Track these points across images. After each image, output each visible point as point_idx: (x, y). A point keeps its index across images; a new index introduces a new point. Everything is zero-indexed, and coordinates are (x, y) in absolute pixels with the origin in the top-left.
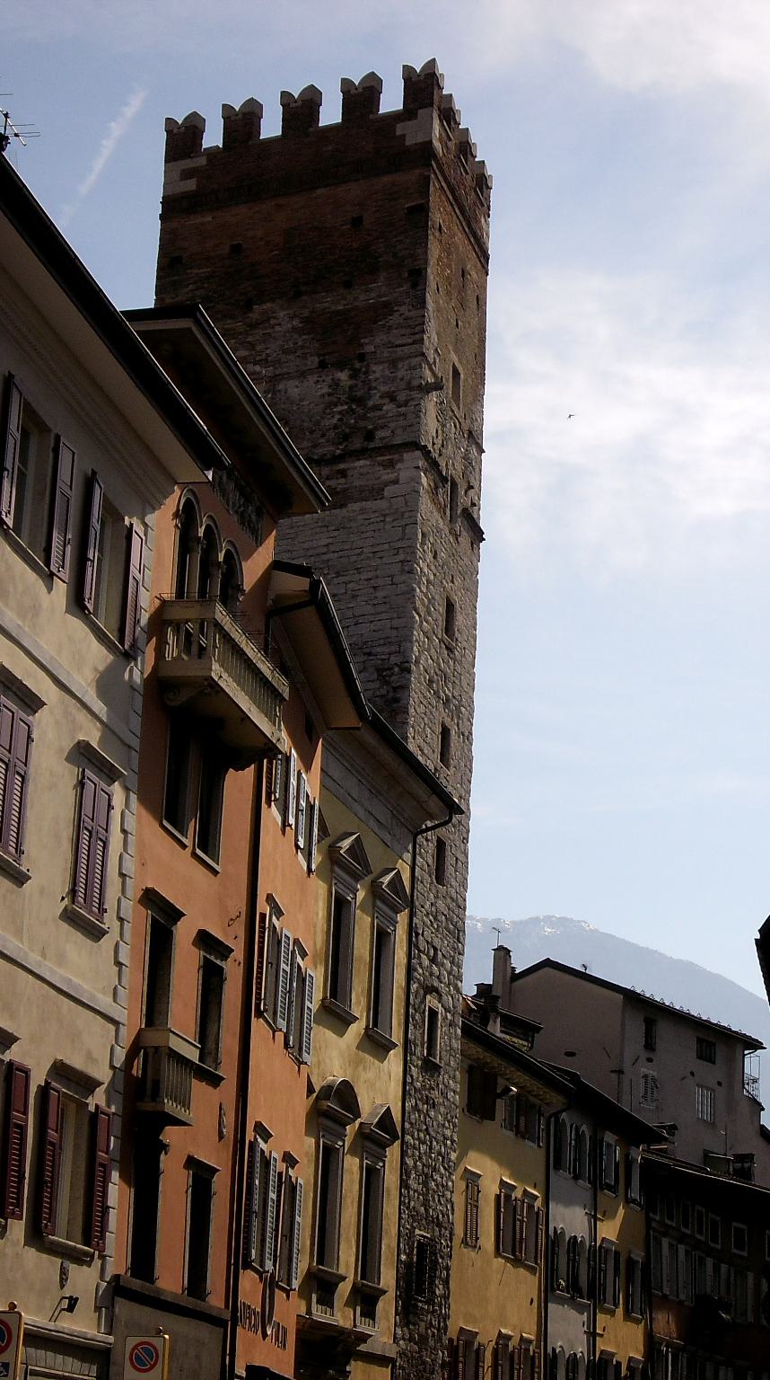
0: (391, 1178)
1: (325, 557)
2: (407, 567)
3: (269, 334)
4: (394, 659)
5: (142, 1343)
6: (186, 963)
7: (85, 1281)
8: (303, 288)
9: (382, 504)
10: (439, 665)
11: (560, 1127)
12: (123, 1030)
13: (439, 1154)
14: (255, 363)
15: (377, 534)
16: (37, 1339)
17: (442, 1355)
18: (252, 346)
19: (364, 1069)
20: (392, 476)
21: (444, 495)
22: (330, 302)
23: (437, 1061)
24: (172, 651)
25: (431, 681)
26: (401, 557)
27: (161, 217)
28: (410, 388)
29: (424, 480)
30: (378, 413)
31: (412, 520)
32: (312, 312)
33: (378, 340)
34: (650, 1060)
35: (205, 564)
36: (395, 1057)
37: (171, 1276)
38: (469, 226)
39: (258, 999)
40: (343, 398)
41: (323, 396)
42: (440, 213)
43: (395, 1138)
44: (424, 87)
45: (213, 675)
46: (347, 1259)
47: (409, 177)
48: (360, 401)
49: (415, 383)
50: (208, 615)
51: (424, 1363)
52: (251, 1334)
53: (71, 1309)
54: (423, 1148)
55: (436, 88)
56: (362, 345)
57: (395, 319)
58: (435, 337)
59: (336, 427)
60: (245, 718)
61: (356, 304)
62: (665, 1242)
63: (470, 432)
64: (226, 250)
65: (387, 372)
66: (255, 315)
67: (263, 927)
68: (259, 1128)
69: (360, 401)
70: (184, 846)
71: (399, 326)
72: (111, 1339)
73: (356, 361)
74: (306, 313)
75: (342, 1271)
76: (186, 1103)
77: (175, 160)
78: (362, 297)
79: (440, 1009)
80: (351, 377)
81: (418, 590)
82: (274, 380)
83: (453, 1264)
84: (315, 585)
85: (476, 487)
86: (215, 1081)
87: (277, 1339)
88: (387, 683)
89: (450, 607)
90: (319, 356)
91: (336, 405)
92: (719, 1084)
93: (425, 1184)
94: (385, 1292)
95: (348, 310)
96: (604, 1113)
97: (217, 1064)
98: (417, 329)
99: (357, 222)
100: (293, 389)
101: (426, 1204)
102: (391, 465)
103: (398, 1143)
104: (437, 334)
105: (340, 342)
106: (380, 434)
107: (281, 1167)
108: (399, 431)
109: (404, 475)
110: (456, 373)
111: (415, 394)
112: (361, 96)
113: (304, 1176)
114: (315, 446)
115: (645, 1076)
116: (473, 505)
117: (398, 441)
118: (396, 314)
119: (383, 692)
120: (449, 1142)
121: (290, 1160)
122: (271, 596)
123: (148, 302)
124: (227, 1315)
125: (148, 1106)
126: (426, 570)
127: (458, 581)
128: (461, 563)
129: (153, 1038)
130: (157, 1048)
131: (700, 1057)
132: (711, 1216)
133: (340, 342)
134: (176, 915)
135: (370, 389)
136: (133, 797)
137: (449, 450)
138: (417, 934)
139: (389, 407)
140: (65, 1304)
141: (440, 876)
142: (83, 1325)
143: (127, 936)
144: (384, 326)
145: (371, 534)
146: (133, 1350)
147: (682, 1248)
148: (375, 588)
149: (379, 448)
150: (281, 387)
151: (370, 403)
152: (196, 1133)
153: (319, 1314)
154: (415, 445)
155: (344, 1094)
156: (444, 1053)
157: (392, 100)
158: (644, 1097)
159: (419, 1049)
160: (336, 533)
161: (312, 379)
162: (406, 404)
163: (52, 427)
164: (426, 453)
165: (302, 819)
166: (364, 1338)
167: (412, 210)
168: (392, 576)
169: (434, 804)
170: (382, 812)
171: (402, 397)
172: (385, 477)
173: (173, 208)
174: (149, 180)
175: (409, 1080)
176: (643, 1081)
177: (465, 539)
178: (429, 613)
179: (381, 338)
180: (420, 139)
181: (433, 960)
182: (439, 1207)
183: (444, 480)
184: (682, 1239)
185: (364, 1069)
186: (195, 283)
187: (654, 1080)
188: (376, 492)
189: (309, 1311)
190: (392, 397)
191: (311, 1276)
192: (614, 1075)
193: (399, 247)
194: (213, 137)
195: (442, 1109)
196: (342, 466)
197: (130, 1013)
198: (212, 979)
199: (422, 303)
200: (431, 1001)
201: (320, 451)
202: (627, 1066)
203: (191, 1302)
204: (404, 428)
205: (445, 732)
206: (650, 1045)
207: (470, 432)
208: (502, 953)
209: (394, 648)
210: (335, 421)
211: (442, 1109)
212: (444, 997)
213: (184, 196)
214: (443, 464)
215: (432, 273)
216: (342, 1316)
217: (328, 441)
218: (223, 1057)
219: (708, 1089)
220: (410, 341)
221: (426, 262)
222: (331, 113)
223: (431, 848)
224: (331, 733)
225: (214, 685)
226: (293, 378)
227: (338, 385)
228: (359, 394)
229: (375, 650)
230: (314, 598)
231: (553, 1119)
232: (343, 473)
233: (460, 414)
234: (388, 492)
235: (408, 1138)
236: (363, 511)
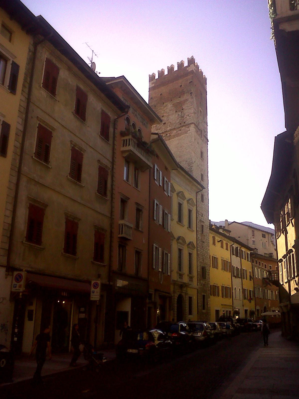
5: (95, 282)
9: (187, 134)
20: (189, 129)
22: (177, 101)
34: (253, 238)
44: (191, 61)
48: (183, 117)
59: (179, 122)
82: (169, 116)
95: (180, 102)
102: (189, 127)
119: (189, 168)
138: (198, 211)
139: (188, 117)
141: (202, 200)
146: (98, 287)
147: (259, 270)
157: (186, 64)
158: (253, 244)
175: (198, 238)
179: (186, 105)
183: (199, 130)
184: (259, 268)
190: (188, 115)
222: (176, 69)
223: (200, 196)
232: (180, 130)
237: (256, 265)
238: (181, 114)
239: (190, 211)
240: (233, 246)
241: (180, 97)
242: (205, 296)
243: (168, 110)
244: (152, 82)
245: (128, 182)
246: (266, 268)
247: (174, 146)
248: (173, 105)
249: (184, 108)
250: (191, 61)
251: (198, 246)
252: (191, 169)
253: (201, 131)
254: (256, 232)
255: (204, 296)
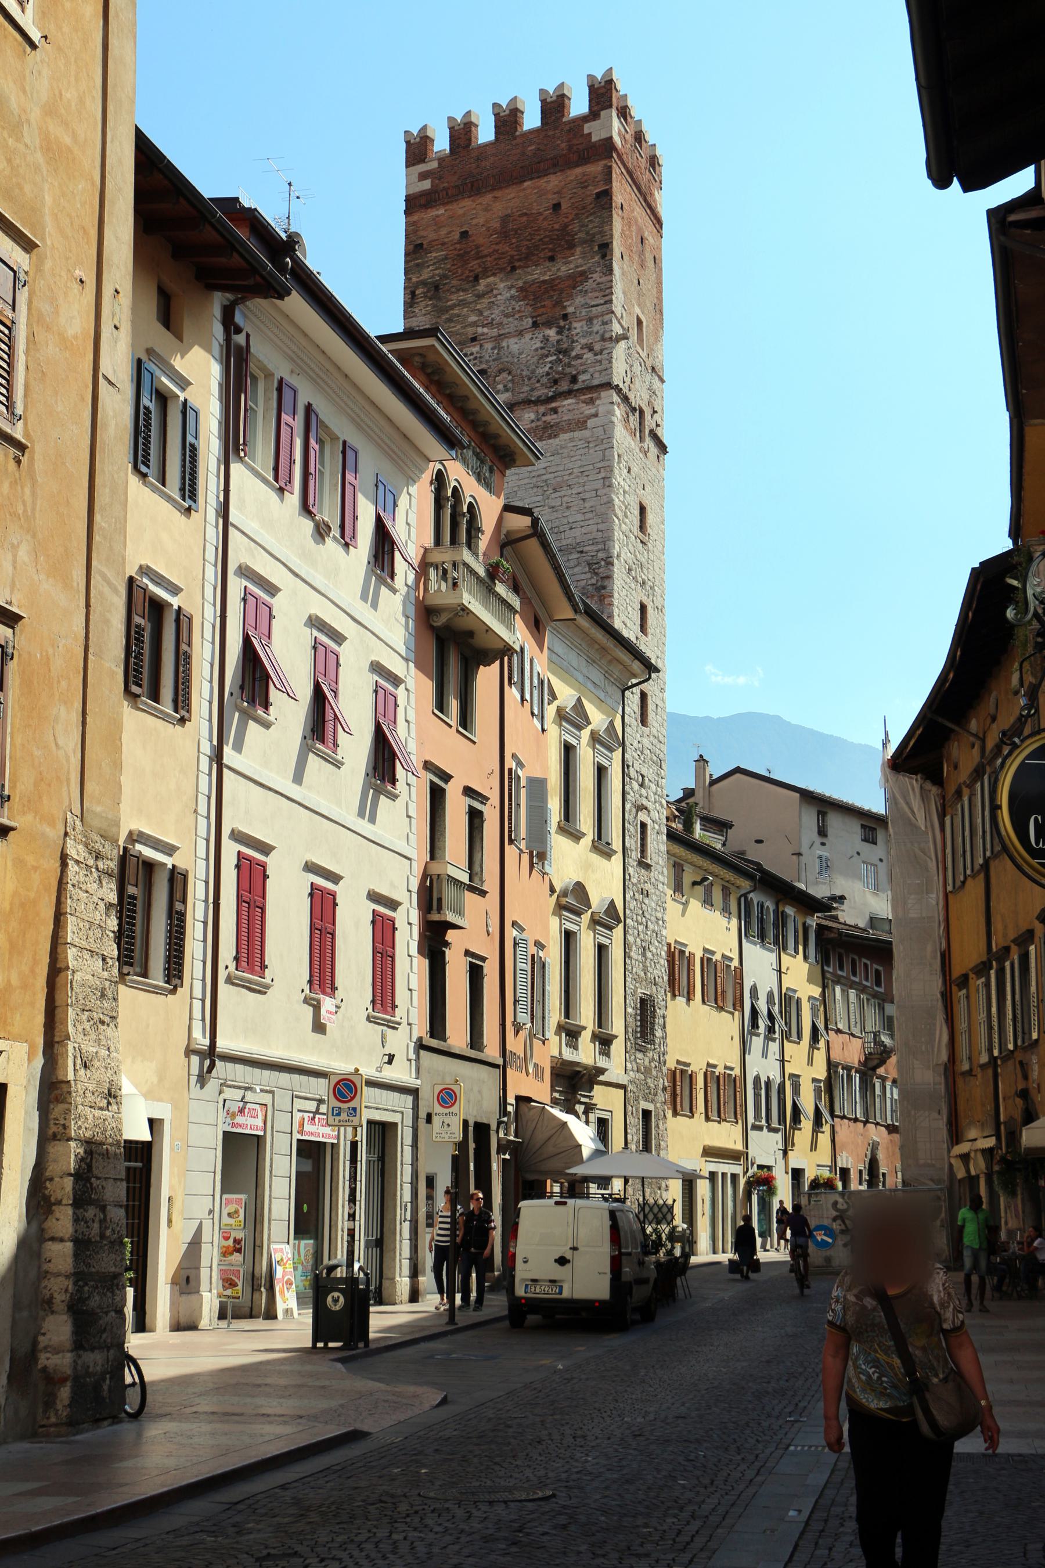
0: (616, 953)
1: (544, 478)
2: (607, 482)
3: (493, 302)
4: (601, 555)
6: (456, 808)
7: (401, 1042)
8: (517, 264)
9: (586, 433)
10: (636, 556)
11: (748, 904)
12: (414, 864)
13: (654, 931)
14: (483, 326)
15: (583, 457)
16: (371, 1083)
17: (664, 1082)
18: (480, 313)
19: (593, 872)
20: (593, 411)
21: (634, 419)
22: (538, 274)
23: (649, 861)
24: (433, 586)
25: (630, 570)
26: (603, 475)
27: (406, 212)
28: (603, 339)
29: (618, 412)
30: (579, 361)
31: (610, 445)
32: (525, 283)
33: (577, 301)
34: (823, 844)
35: (454, 519)
36: (617, 859)
37: (457, 1035)
38: (645, 200)
39: (510, 831)
40: (552, 350)
41: (536, 350)
42: (621, 192)
43: (619, 921)
44: (603, 93)
45: (464, 602)
46: (586, 1015)
47: (595, 169)
48: (566, 352)
49: (607, 336)
50: (457, 558)
51: (649, 1088)
52: (518, 1073)
53: (390, 1062)
54: (641, 928)
55: (614, 91)
56: (565, 307)
57: (589, 284)
58: (621, 296)
59: (548, 374)
60: (489, 630)
61: (559, 274)
62: (838, 989)
63: (653, 368)
64: (457, 236)
65: (585, 328)
66: (482, 286)
67: (510, 778)
68: (514, 924)
69: (566, 352)
70: (450, 726)
71: (594, 290)
72: (419, 1082)
73: (562, 320)
74: (520, 283)
75: (583, 1023)
76: (461, 913)
77: (414, 165)
78: (563, 268)
79: (649, 822)
80: (559, 333)
81: (617, 500)
82: (500, 337)
83: (669, 1013)
84: (535, 522)
85: (660, 411)
86: (483, 893)
87: (537, 1075)
88: (596, 574)
89: (642, 509)
90: (532, 317)
91: (547, 356)
92: (881, 860)
93: (644, 955)
94: (616, 1037)
95: (553, 280)
96: (784, 891)
97: (482, 882)
98: (606, 292)
99: (557, 207)
100: (513, 345)
101: (645, 970)
102: (591, 401)
103: (621, 925)
104: (624, 293)
105: (548, 305)
106: (582, 378)
107: (532, 950)
108: (596, 375)
109: (602, 410)
110: (640, 322)
111: (607, 344)
112: (554, 106)
113: (553, 956)
114: (532, 390)
115: (820, 857)
116: (658, 425)
117: (596, 382)
118: (591, 281)
119: (594, 581)
120: (661, 922)
121: (539, 945)
122: (504, 531)
123: (399, 327)
124: (500, 1062)
125: (435, 917)
126: (622, 483)
127: (648, 488)
128: (650, 473)
129: (436, 869)
130: (439, 875)
131: (865, 840)
132: (875, 966)
133: (548, 305)
134: (447, 777)
135: (573, 342)
136: (412, 665)
137: (637, 383)
138: (628, 766)
139: (588, 356)
140: (386, 1059)
142: (401, 1073)
143: (414, 829)
144: (581, 291)
145: (579, 457)
148: (583, 500)
149: (582, 389)
150: (504, 344)
151: (573, 354)
152: (471, 932)
153: (568, 1055)
154: (608, 385)
155: (580, 890)
156: (654, 855)
157: (579, 105)
159: (634, 853)
160: (552, 458)
161: (528, 336)
162: (601, 352)
163: (339, 435)
164: (618, 390)
165: (535, 693)
166: (602, 1071)
167: (599, 195)
168: (596, 490)
169: (636, 666)
170: (596, 675)
171: (597, 347)
172: (587, 412)
173: (414, 204)
174: (394, 182)
175: (627, 877)
176: (818, 861)
177: (654, 450)
178: (627, 517)
179: (579, 300)
180: (604, 135)
181: (642, 785)
182: (656, 971)
183: (634, 410)
185: (593, 872)
186: (434, 264)
187: (827, 860)
188: (581, 424)
189: (560, 1053)
191: (560, 1028)
192: (795, 857)
193: (590, 226)
194: (442, 143)
195: (654, 898)
196: (554, 405)
197: (417, 849)
198: (475, 818)
199: (610, 271)
200: (642, 816)
201: (536, 394)
202: (804, 850)
203: (473, 1054)
204: (600, 372)
205: (643, 608)
206: (822, 832)
207: (653, 368)
208: (702, 763)
209: (601, 546)
210: (547, 369)
211: (654, 898)
212: (652, 812)
213: (423, 194)
214: (631, 396)
215: (617, 247)
216: (586, 1054)
217: (542, 385)
218: (485, 876)
219: (872, 865)
220: (602, 301)
221: (612, 236)
223: (637, 698)
224: (553, 624)
225: (464, 609)
226: (514, 336)
227: (548, 340)
228: (565, 346)
229: (586, 549)
230: (536, 531)
231: (743, 899)
232: (555, 411)
233: (644, 355)
234: (590, 423)
235: (628, 921)
236: (572, 440)
237: (839, 973)
238: (559, 337)
239: (601, 772)
240: (751, 895)
241: (552, 259)
242: (650, 1112)
243: (496, 314)
244: (422, 168)
245: (164, 485)
246: (878, 983)
247: (526, 481)
248: (521, 289)
249: (570, 310)
250: (603, 93)
251: (628, 911)
252: (604, 588)
253: (642, 412)
254: (834, 821)
255: (647, 1114)
